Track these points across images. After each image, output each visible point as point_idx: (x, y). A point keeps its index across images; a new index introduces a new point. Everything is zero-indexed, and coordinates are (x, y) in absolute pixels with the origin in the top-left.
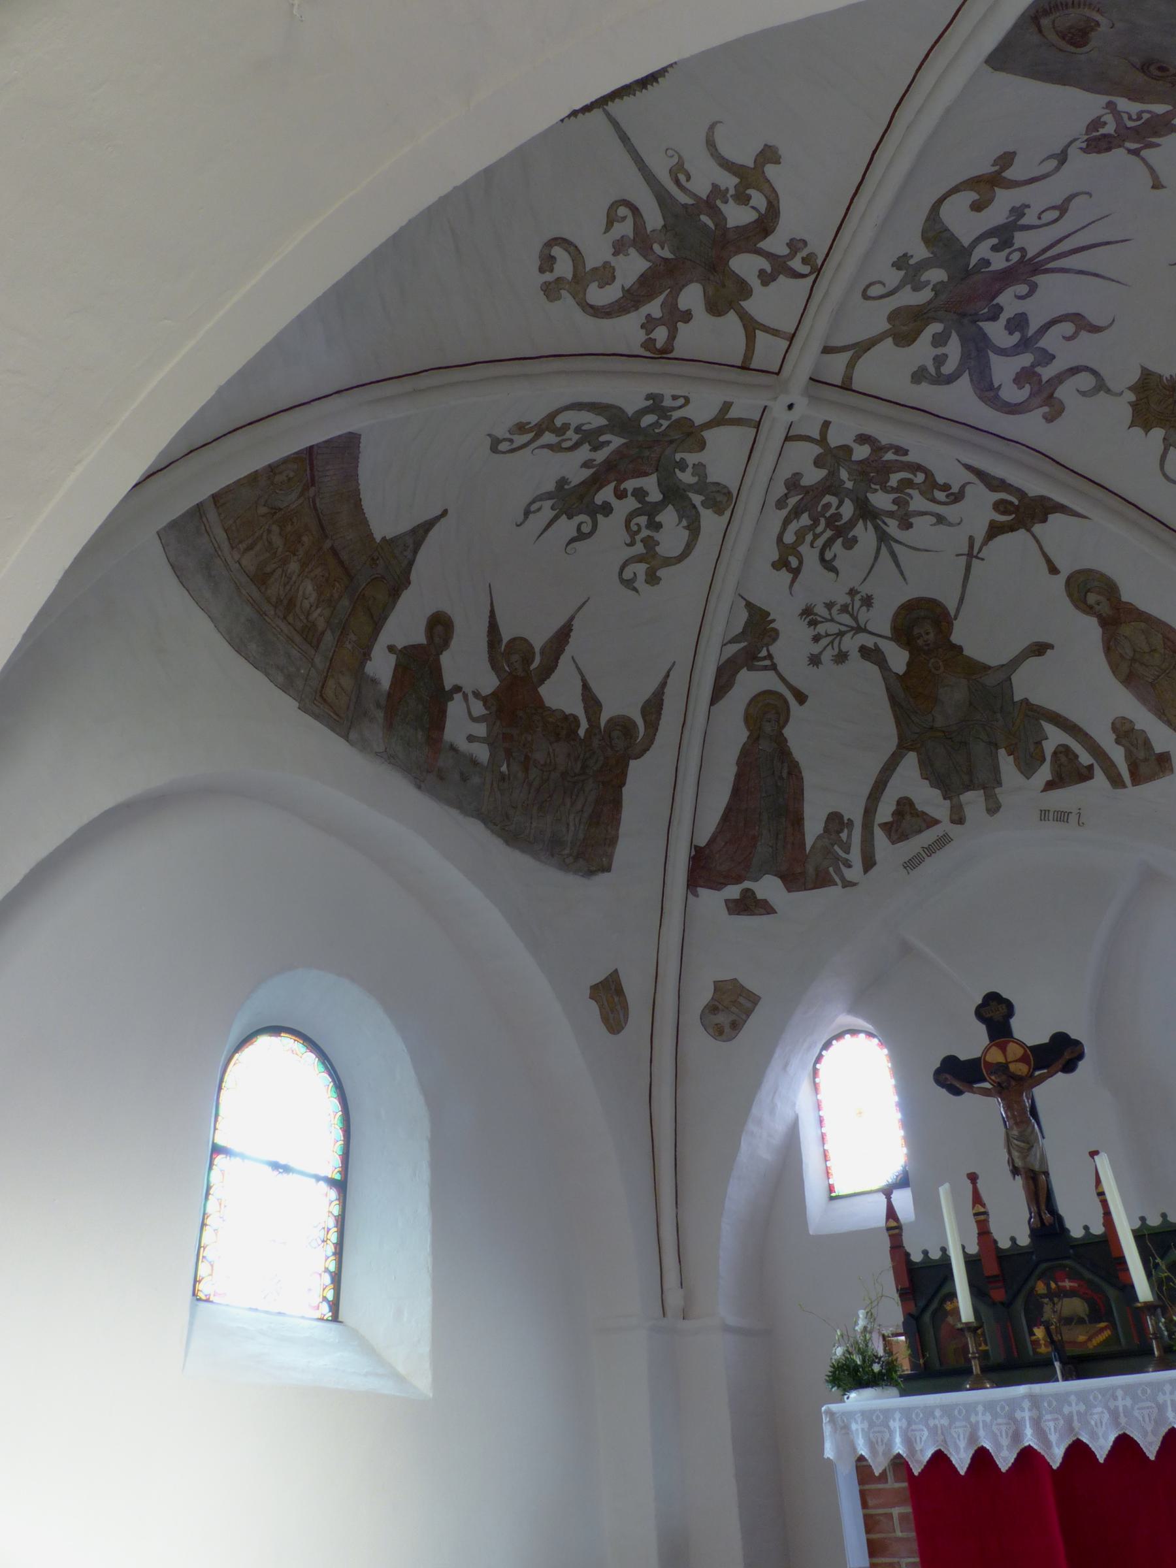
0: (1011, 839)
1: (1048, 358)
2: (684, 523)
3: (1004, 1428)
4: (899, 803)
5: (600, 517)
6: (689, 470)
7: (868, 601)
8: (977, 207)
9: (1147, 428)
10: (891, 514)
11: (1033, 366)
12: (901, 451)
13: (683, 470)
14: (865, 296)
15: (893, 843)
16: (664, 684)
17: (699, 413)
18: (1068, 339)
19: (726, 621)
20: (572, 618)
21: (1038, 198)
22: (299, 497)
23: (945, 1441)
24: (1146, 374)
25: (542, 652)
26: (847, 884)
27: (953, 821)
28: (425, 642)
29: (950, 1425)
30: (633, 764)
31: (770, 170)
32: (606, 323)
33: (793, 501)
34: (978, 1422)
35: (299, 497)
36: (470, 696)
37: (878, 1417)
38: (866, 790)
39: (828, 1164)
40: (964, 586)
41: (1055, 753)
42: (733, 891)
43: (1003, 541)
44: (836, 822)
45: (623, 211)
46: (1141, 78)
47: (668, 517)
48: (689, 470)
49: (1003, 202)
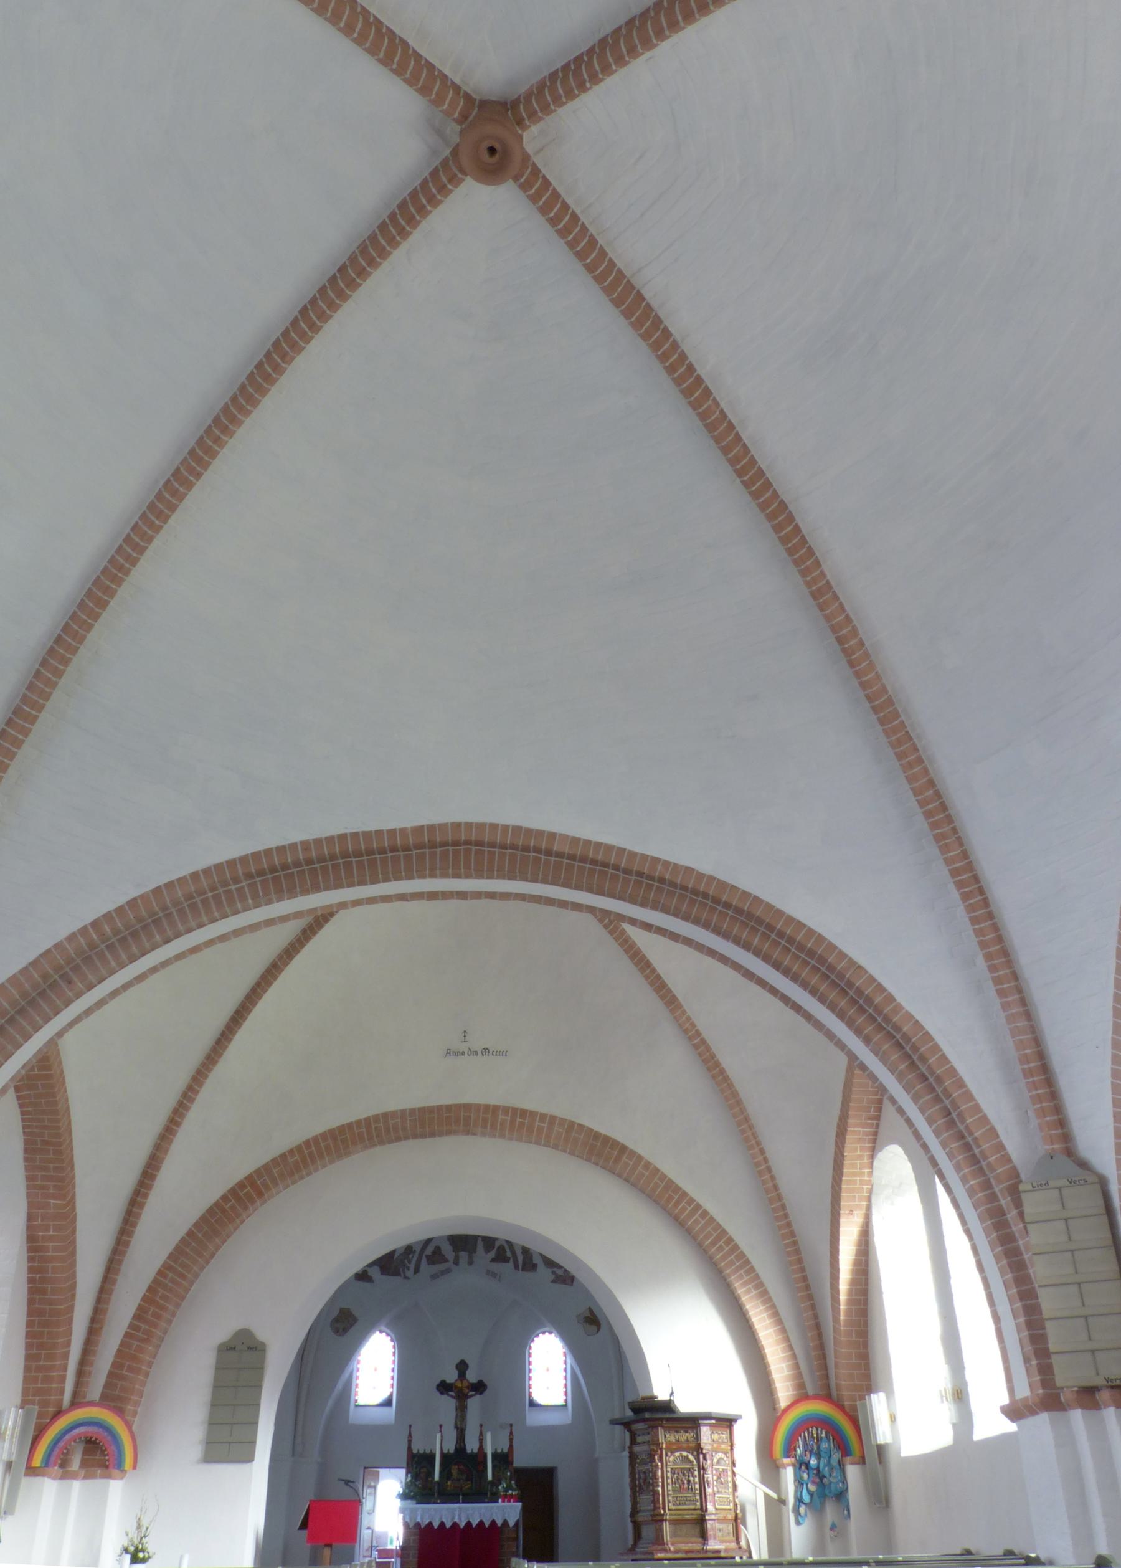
26: (406, 1278)
28: (515, 1465)
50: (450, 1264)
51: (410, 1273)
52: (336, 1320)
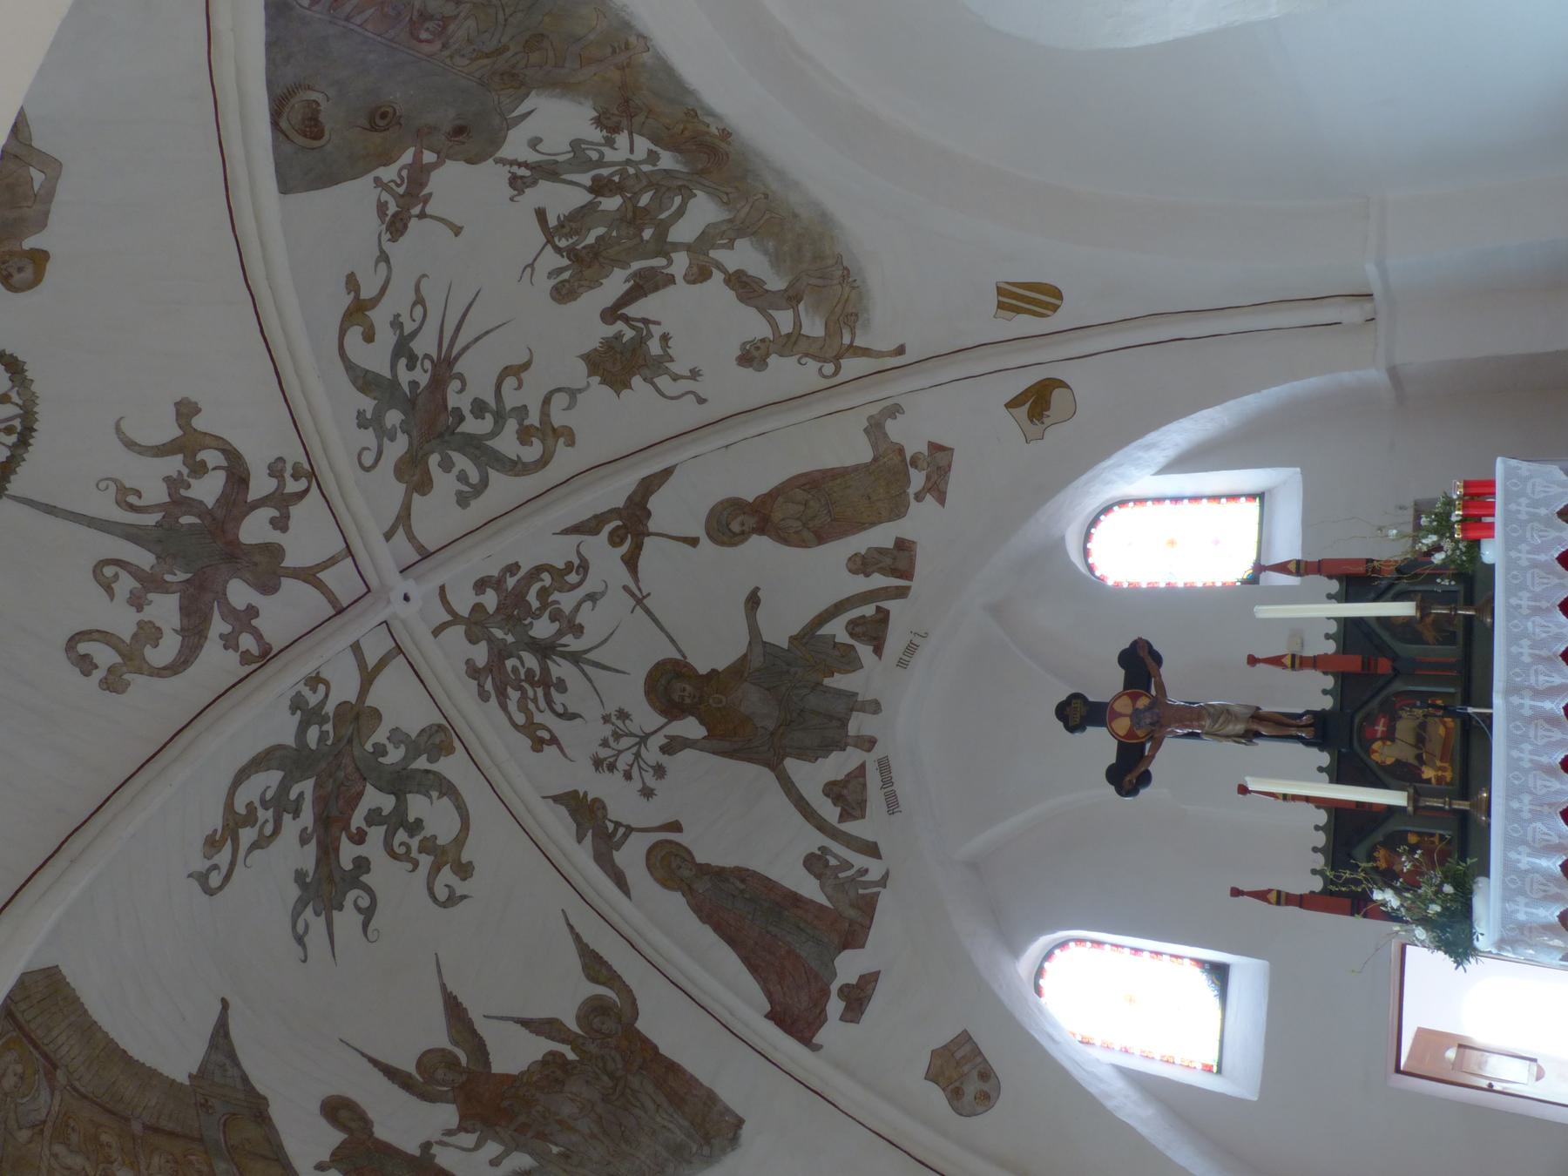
0: (910, 707)
1: (522, 411)
2: (435, 794)
3: (1541, 732)
4: (827, 795)
5: (364, 878)
6: (390, 747)
7: (623, 715)
8: (369, 337)
9: (627, 385)
10: (560, 633)
11: (520, 424)
12: (513, 568)
13: (384, 753)
14: (367, 470)
15: (863, 817)
16: (577, 938)
17: (344, 688)
18: (520, 386)
19: (558, 826)
20: (443, 987)
21: (397, 302)
22: (52, 1094)
23: (1551, 805)
24: (587, 358)
25: (456, 1044)
26: (883, 882)
27: (869, 750)
29: (1531, 793)
30: (640, 1025)
31: (199, 423)
32: (191, 670)
33: (489, 685)
34: (1531, 761)
35: (52, 1094)
36: (446, 1139)
37: (1513, 881)
38: (798, 818)
39: (1178, 1061)
40: (662, 629)
41: (852, 635)
42: (835, 1006)
43: (643, 562)
44: (815, 863)
45: (109, 571)
46: (377, 138)
47: (417, 806)
48: (390, 747)
49: (380, 317)
50: (870, 760)
51: (875, 869)
52: (955, 1095)
